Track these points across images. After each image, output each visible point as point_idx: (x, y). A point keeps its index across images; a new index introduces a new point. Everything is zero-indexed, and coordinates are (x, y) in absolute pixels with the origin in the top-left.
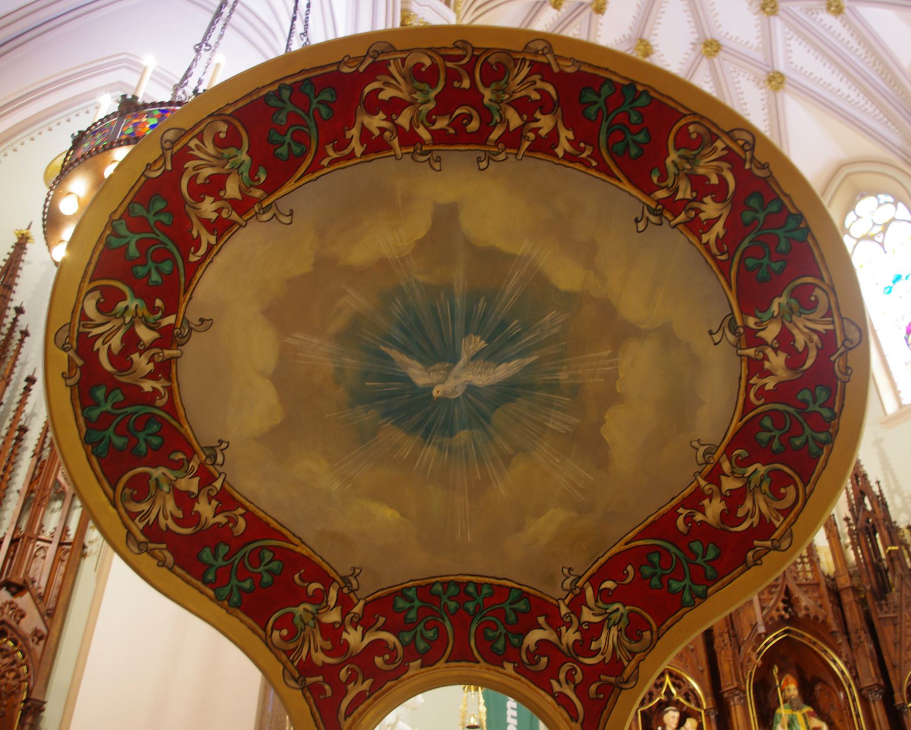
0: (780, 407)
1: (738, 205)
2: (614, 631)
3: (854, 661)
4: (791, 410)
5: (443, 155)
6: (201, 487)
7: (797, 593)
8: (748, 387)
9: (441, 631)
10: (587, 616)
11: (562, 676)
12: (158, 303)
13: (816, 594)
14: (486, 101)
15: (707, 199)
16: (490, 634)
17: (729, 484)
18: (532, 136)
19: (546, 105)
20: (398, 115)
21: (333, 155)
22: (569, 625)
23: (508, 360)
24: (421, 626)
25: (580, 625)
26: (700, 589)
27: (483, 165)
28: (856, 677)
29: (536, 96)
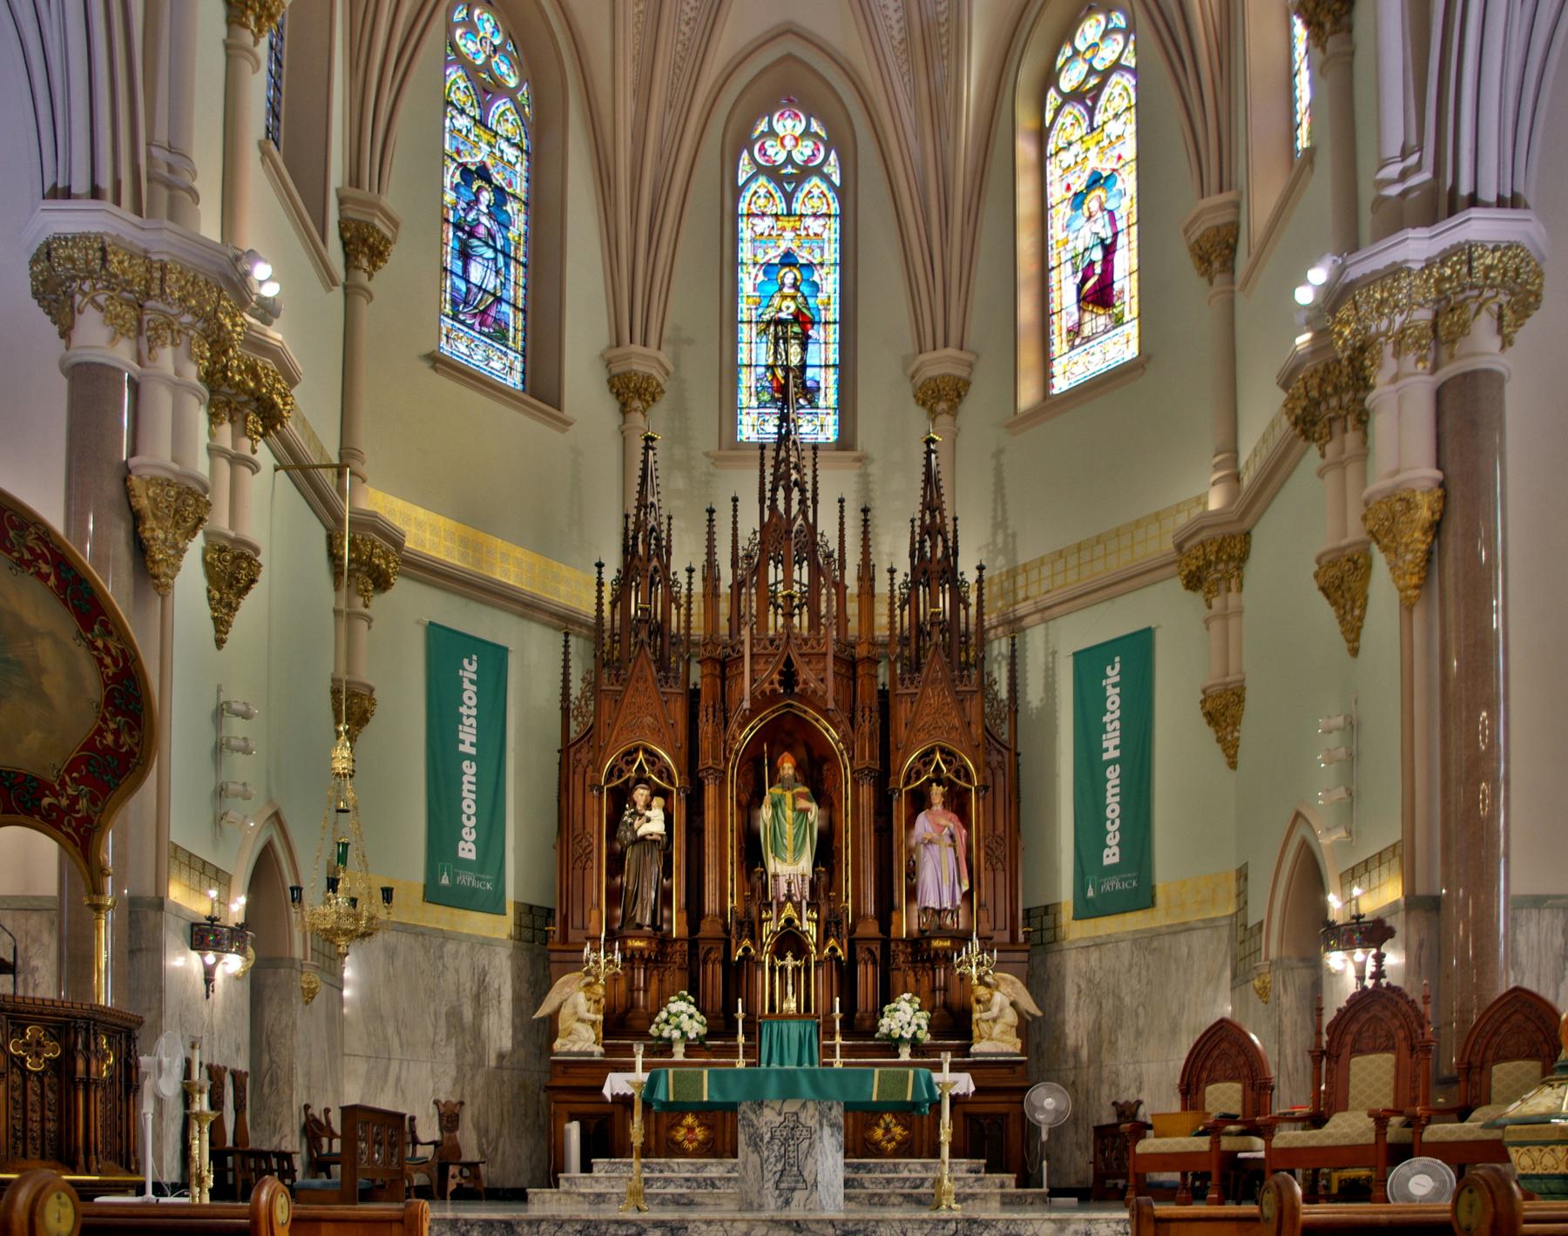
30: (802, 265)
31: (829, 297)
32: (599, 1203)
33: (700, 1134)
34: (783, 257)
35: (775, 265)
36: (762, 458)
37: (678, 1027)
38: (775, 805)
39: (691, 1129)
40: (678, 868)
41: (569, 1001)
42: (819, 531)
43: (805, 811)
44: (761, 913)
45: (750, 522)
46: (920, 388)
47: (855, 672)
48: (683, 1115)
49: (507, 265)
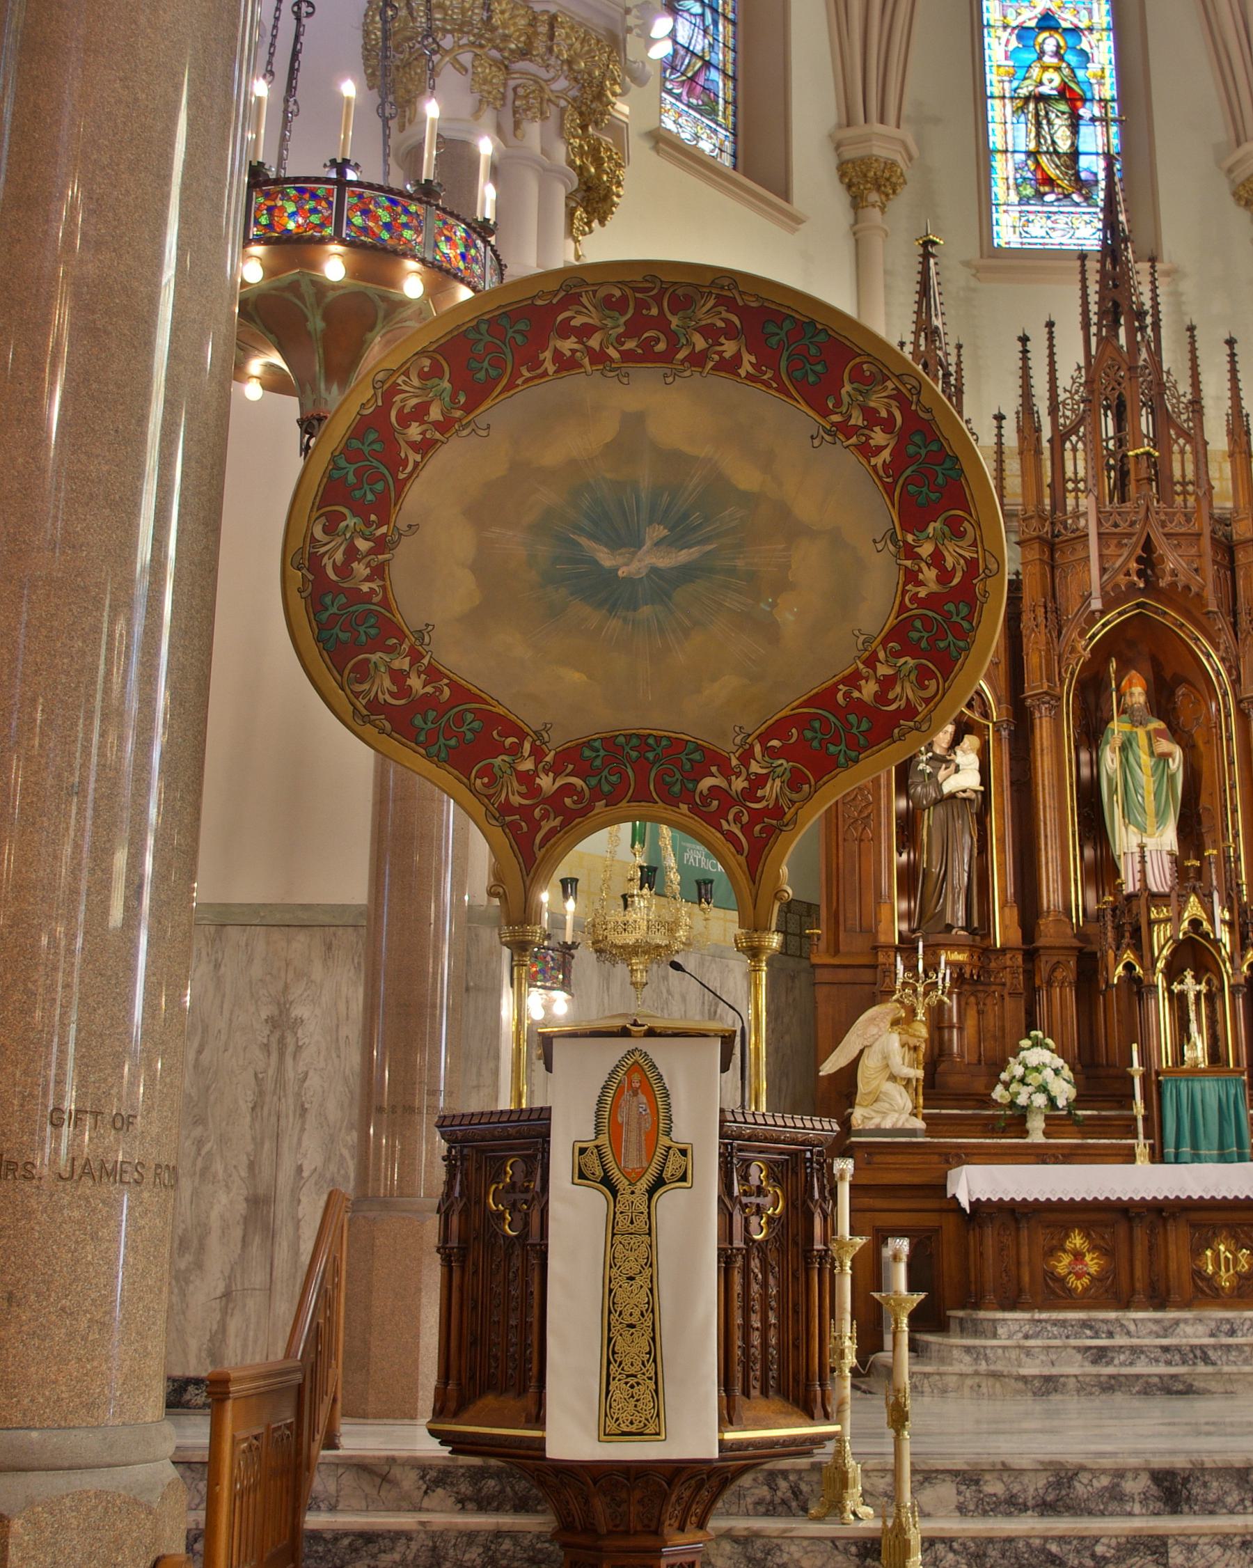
0: (930, 614)
1: (903, 439)
2: (778, 782)
3: (1238, 658)
4: (939, 618)
5: (630, 371)
6: (411, 665)
7: (1162, 547)
8: (904, 592)
9: (624, 776)
10: (755, 768)
11: (731, 817)
12: (373, 517)
13: (1194, 551)
14: (673, 327)
15: (877, 429)
16: (668, 779)
17: (883, 670)
18: (716, 357)
19: (730, 332)
20: (589, 338)
21: (527, 374)
22: (738, 775)
23: (690, 547)
24: (605, 773)
25: (748, 775)
26: (853, 754)
27: (670, 380)
28: (1236, 682)
29: (721, 324)
30: (1065, 30)
31: (1103, 70)
32: (1048, 1393)
33: (1092, 1263)
34: (1040, 20)
35: (1032, 29)
36: (1083, 271)
37: (1043, 1089)
38: (1125, 748)
39: (1078, 1256)
40: (1001, 840)
41: (877, 1046)
42: (1165, 368)
43: (1164, 757)
44: (1149, 911)
45: (1071, 356)
46: (1243, 185)
47: (1232, 560)
48: (1066, 1232)
49: (715, 23)
